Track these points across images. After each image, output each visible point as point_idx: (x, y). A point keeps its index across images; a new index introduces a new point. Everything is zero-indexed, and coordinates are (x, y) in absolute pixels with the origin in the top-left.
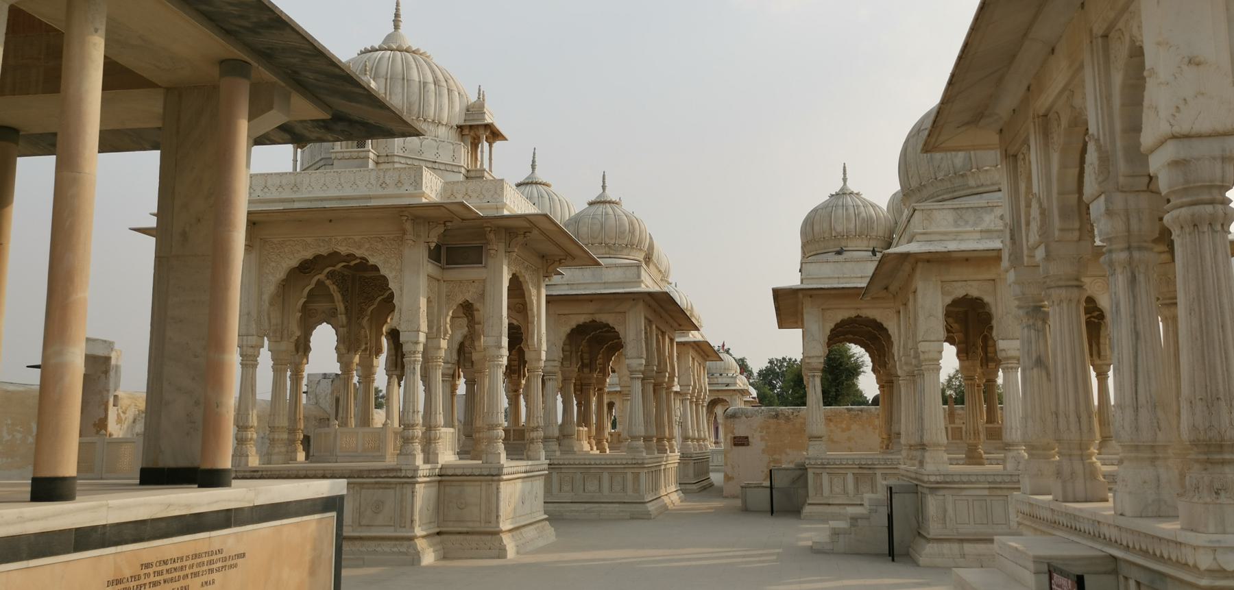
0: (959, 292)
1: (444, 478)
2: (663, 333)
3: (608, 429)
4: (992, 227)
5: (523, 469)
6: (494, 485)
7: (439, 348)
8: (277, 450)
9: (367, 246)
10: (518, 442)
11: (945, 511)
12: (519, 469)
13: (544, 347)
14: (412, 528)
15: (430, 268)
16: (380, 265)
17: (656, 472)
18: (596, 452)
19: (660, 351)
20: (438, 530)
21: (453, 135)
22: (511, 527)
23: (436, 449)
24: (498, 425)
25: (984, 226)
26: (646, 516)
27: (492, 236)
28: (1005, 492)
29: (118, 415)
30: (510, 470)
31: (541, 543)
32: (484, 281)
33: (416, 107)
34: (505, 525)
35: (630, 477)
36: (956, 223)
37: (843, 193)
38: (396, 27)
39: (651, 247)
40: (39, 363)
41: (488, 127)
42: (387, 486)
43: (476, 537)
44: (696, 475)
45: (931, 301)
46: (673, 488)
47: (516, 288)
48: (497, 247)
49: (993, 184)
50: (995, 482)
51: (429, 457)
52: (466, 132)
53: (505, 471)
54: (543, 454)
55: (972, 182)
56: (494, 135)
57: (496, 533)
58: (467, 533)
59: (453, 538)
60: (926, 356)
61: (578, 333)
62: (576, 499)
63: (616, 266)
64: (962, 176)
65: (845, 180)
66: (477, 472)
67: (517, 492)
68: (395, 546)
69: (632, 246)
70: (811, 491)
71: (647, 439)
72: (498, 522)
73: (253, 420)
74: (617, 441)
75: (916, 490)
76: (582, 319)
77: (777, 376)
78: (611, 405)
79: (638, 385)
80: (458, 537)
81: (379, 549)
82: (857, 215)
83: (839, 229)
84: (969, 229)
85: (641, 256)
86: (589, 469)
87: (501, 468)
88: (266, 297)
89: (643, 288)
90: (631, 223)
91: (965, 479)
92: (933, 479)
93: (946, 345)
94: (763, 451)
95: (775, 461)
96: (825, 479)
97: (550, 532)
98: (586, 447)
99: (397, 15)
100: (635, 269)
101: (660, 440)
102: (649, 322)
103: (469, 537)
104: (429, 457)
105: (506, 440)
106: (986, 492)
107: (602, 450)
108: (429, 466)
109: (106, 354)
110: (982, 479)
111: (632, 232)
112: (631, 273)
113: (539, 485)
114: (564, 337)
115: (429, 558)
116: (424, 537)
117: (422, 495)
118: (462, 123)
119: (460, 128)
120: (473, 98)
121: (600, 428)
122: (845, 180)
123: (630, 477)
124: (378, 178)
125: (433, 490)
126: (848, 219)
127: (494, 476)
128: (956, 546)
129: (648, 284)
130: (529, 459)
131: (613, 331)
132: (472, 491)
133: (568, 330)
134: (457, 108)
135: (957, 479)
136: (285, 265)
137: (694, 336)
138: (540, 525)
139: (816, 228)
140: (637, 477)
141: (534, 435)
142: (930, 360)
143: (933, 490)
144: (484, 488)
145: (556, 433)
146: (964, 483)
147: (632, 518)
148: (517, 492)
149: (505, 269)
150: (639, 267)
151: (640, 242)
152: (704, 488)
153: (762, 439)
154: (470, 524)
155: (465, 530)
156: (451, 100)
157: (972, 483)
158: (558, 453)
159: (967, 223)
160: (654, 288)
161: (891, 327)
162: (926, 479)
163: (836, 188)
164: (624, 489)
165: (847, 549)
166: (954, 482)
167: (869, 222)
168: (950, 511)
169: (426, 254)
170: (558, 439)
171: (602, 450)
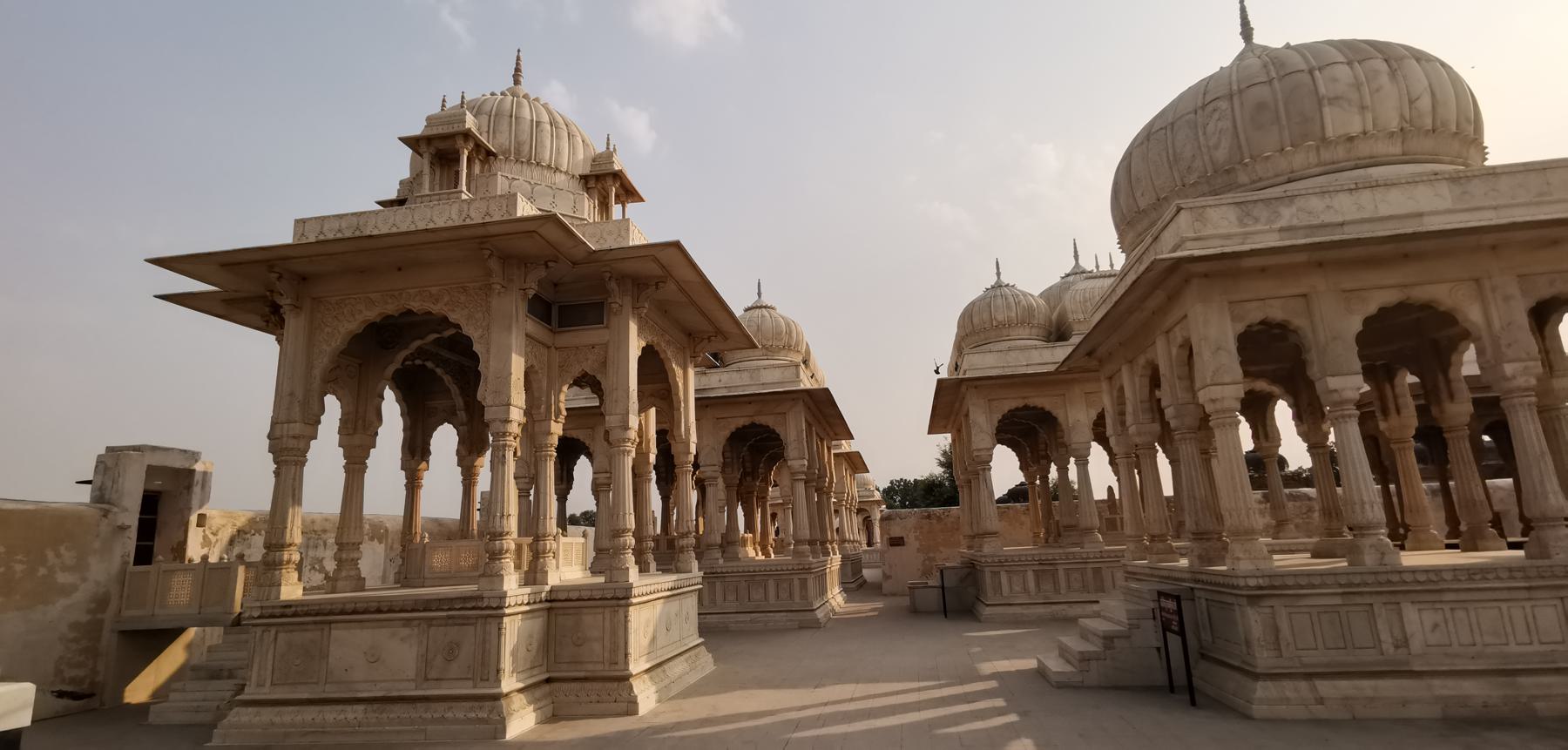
0: (1255, 314)
1: (558, 608)
2: (822, 440)
3: (772, 536)
4: (1295, 222)
5: (670, 585)
6: (621, 611)
7: (549, 433)
8: (344, 574)
9: (446, 299)
10: (664, 552)
11: (1277, 631)
12: (659, 587)
13: (694, 438)
14: (498, 681)
15: (532, 326)
16: (463, 323)
17: (822, 577)
18: (761, 557)
19: (821, 458)
20: (546, 676)
21: (575, 186)
22: (648, 666)
23: (544, 565)
24: (625, 531)
25: (1283, 223)
26: (815, 625)
27: (613, 285)
28: (1368, 600)
29: (205, 537)
30: (644, 590)
31: (693, 678)
32: (606, 345)
33: (526, 148)
34: (637, 665)
35: (796, 582)
36: (1241, 222)
37: (998, 285)
38: (517, 82)
39: (808, 352)
40: (90, 478)
41: (618, 176)
42: (465, 622)
43: (597, 685)
44: (854, 574)
45: (1214, 331)
46: (837, 590)
47: (652, 363)
48: (620, 300)
49: (1277, 176)
50: (1350, 585)
51: (533, 576)
52: (592, 184)
53: (635, 592)
54: (695, 565)
55: (1243, 178)
56: (629, 193)
57: (625, 678)
58: (586, 679)
59: (565, 686)
60: (1218, 406)
61: (737, 439)
62: (744, 613)
63: (775, 367)
64: (1228, 172)
65: (998, 274)
66: (598, 595)
67: (656, 613)
68: (472, 709)
69: (788, 348)
70: (990, 592)
71: (811, 543)
72: (626, 663)
73: (295, 535)
74: (780, 547)
75: (1224, 594)
76: (741, 422)
77: (896, 493)
78: (774, 516)
79: (801, 487)
80: (573, 685)
81: (449, 715)
82: (1018, 304)
83: (1000, 317)
84: (1259, 227)
85: (798, 359)
86: (755, 576)
87: (630, 587)
88: (317, 372)
89: (802, 387)
90: (788, 325)
91: (1303, 582)
92: (1252, 582)
93: (1094, 444)
94: (919, 550)
95: (929, 559)
96: (1004, 578)
97: (706, 663)
98: (751, 552)
99: (517, 70)
100: (793, 369)
101: (823, 543)
102: (809, 425)
103: (588, 685)
104: (533, 576)
105: (656, 550)
106: (1338, 601)
107: (767, 554)
108: (528, 590)
109: (187, 465)
110: (1330, 580)
111: (790, 334)
112: (789, 373)
113: (691, 604)
114: (723, 441)
115: (522, 721)
116: (520, 691)
117: (513, 632)
118: (587, 171)
119: (584, 179)
120: (601, 149)
121: (765, 534)
122: (998, 274)
123: (796, 582)
124: (460, 211)
125: (537, 624)
126: (1009, 307)
127: (620, 599)
128: (1303, 685)
129: (806, 383)
130: (678, 571)
131: (776, 439)
132: (593, 622)
133: (727, 433)
134: (581, 156)
135: (1290, 582)
136: (342, 330)
137: (846, 446)
138: (692, 653)
139: (976, 320)
140: (804, 583)
141: (684, 542)
142: (1224, 411)
143: (1254, 600)
144: (608, 616)
145: (719, 540)
146: (1302, 587)
147: (801, 628)
148: (656, 613)
149: (633, 328)
150: (797, 366)
151: (797, 344)
152: (861, 586)
153: (917, 538)
154: (590, 667)
155: (582, 674)
156: (572, 146)
157: (1313, 586)
158: (721, 561)
159: (1257, 220)
160: (809, 386)
161: (1059, 414)
162: (1242, 583)
163: (993, 280)
164: (791, 595)
165: (1106, 680)
166: (1237, 587)
167: (1030, 310)
168: (1284, 626)
169: (523, 308)
170: (721, 546)
171: (767, 554)
